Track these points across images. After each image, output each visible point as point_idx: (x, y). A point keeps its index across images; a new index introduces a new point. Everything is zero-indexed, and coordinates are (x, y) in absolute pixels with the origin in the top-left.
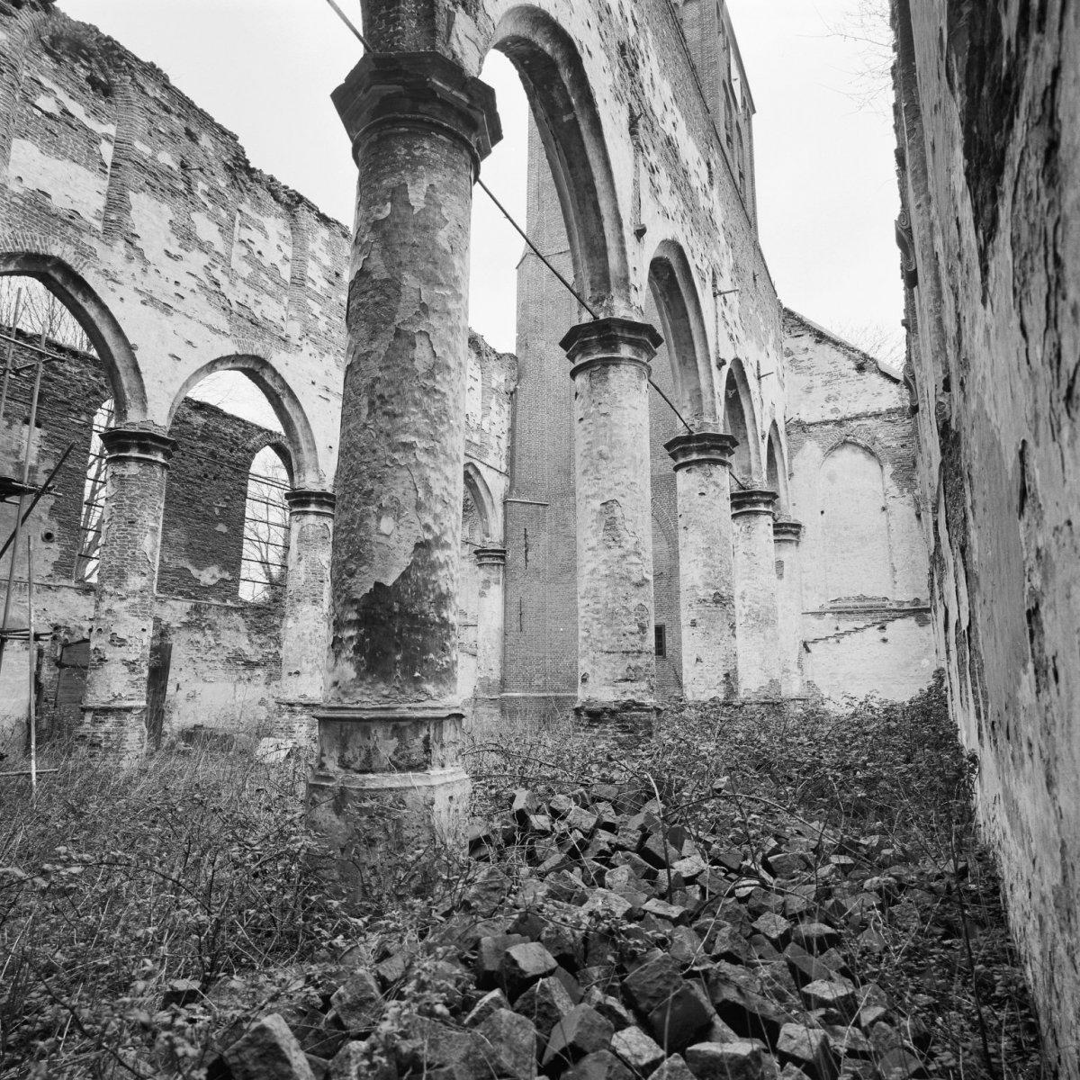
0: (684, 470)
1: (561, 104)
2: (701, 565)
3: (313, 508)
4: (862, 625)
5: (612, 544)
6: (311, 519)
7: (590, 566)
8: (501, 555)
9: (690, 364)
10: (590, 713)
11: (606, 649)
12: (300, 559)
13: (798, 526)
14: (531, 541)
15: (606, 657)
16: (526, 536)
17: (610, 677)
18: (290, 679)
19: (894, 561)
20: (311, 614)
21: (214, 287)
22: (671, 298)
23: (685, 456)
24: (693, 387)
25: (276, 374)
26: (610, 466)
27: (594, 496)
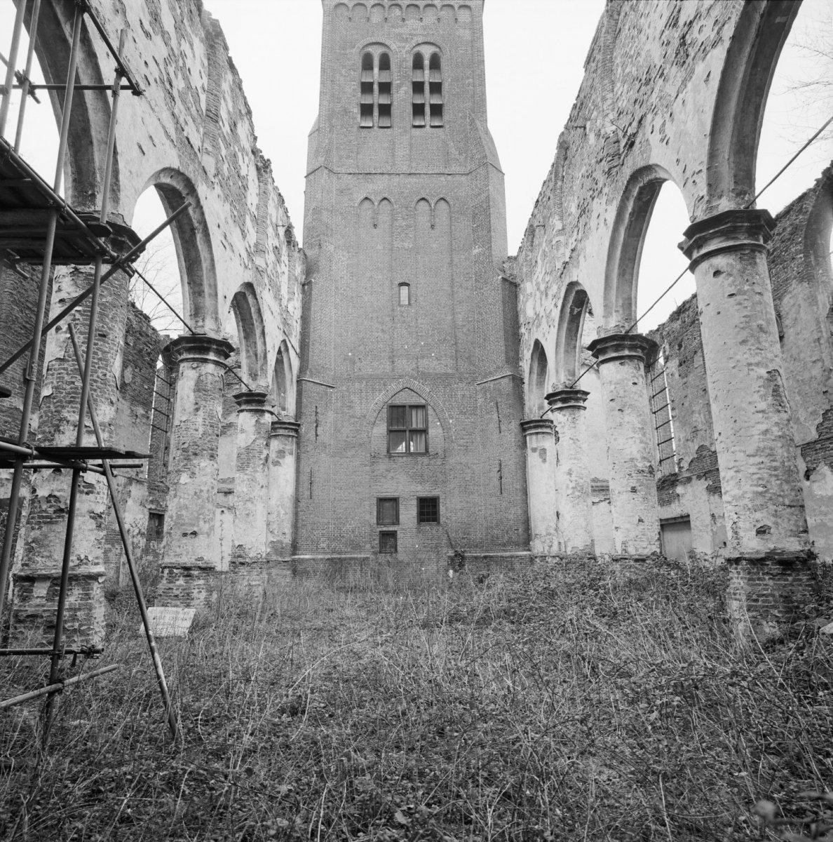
0: (617, 363)
2: (638, 441)
3: (212, 356)
4: (597, 500)
5: (780, 408)
6: (210, 368)
8: (295, 427)
9: (627, 277)
10: (781, 562)
11: (787, 502)
12: (197, 410)
14: (320, 417)
15: (789, 510)
16: (317, 413)
17: (794, 529)
18: (184, 540)
20: (209, 470)
21: (168, 87)
22: (636, 219)
23: (616, 351)
24: (625, 296)
25: (199, 206)
26: (769, 339)
27: (757, 364)
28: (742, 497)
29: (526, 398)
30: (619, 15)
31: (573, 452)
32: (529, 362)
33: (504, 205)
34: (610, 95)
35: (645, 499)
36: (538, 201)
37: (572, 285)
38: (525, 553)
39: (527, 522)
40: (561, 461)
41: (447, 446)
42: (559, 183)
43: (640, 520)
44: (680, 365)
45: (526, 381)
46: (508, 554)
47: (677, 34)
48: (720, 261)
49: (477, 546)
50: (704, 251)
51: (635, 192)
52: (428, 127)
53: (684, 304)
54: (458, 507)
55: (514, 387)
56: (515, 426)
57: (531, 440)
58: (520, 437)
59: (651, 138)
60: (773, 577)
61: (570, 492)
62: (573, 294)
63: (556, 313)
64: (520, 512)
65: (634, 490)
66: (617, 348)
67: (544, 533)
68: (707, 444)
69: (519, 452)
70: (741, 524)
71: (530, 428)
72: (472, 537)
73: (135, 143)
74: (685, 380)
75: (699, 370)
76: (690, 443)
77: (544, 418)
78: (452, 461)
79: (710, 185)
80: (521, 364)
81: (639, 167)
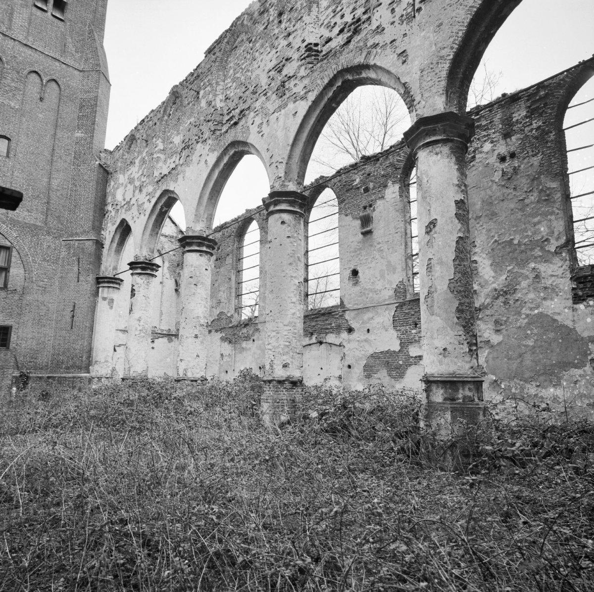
0: (198, 254)
1: (338, 99)
7: (293, 311)
9: (213, 201)
13: (122, 281)
19: (162, 309)
23: (199, 246)
24: (210, 212)
28: (278, 347)
29: (104, 259)
30: (238, 37)
31: (144, 305)
32: (112, 234)
33: (107, 108)
34: (222, 83)
35: (202, 342)
36: (143, 121)
37: (166, 191)
38: (85, 375)
39: (90, 351)
40: (134, 311)
41: (26, 284)
42: (166, 118)
43: (198, 356)
44: (217, 260)
45: (106, 246)
46: (70, 375)
47: (280, 78)
48: (286, 217)
49: (42, 369)
50: (278, 208)
51: (232, 152)
52: (49, 14)
53: (226, 223)
54: (30, 336)
55: (96, 249)
56: (91, 278)
57: (103, 291)
58: (94, 288)
59: (251, 127)
60: (287, 390)
61: (137, 333)
62: (166, 198)
63: (149, 207)
64: (86, 343)
65: (196, 337)
66: (200, 245)
67: (103, 360)
68: (225, 311)
69: (92, 299)
70: (275, 362)
71: (104, 282)
72: (39, 361)
73: (69, 15)
74: (218, 270)
75: (228, 266)
76: (214, 309)
77: (116, 276)
78: (29, 298)
79: (286, 173)
80: (102, 232)
81: (239, 139)
